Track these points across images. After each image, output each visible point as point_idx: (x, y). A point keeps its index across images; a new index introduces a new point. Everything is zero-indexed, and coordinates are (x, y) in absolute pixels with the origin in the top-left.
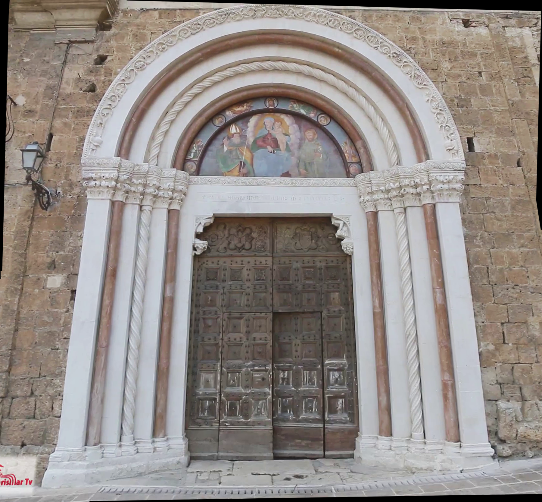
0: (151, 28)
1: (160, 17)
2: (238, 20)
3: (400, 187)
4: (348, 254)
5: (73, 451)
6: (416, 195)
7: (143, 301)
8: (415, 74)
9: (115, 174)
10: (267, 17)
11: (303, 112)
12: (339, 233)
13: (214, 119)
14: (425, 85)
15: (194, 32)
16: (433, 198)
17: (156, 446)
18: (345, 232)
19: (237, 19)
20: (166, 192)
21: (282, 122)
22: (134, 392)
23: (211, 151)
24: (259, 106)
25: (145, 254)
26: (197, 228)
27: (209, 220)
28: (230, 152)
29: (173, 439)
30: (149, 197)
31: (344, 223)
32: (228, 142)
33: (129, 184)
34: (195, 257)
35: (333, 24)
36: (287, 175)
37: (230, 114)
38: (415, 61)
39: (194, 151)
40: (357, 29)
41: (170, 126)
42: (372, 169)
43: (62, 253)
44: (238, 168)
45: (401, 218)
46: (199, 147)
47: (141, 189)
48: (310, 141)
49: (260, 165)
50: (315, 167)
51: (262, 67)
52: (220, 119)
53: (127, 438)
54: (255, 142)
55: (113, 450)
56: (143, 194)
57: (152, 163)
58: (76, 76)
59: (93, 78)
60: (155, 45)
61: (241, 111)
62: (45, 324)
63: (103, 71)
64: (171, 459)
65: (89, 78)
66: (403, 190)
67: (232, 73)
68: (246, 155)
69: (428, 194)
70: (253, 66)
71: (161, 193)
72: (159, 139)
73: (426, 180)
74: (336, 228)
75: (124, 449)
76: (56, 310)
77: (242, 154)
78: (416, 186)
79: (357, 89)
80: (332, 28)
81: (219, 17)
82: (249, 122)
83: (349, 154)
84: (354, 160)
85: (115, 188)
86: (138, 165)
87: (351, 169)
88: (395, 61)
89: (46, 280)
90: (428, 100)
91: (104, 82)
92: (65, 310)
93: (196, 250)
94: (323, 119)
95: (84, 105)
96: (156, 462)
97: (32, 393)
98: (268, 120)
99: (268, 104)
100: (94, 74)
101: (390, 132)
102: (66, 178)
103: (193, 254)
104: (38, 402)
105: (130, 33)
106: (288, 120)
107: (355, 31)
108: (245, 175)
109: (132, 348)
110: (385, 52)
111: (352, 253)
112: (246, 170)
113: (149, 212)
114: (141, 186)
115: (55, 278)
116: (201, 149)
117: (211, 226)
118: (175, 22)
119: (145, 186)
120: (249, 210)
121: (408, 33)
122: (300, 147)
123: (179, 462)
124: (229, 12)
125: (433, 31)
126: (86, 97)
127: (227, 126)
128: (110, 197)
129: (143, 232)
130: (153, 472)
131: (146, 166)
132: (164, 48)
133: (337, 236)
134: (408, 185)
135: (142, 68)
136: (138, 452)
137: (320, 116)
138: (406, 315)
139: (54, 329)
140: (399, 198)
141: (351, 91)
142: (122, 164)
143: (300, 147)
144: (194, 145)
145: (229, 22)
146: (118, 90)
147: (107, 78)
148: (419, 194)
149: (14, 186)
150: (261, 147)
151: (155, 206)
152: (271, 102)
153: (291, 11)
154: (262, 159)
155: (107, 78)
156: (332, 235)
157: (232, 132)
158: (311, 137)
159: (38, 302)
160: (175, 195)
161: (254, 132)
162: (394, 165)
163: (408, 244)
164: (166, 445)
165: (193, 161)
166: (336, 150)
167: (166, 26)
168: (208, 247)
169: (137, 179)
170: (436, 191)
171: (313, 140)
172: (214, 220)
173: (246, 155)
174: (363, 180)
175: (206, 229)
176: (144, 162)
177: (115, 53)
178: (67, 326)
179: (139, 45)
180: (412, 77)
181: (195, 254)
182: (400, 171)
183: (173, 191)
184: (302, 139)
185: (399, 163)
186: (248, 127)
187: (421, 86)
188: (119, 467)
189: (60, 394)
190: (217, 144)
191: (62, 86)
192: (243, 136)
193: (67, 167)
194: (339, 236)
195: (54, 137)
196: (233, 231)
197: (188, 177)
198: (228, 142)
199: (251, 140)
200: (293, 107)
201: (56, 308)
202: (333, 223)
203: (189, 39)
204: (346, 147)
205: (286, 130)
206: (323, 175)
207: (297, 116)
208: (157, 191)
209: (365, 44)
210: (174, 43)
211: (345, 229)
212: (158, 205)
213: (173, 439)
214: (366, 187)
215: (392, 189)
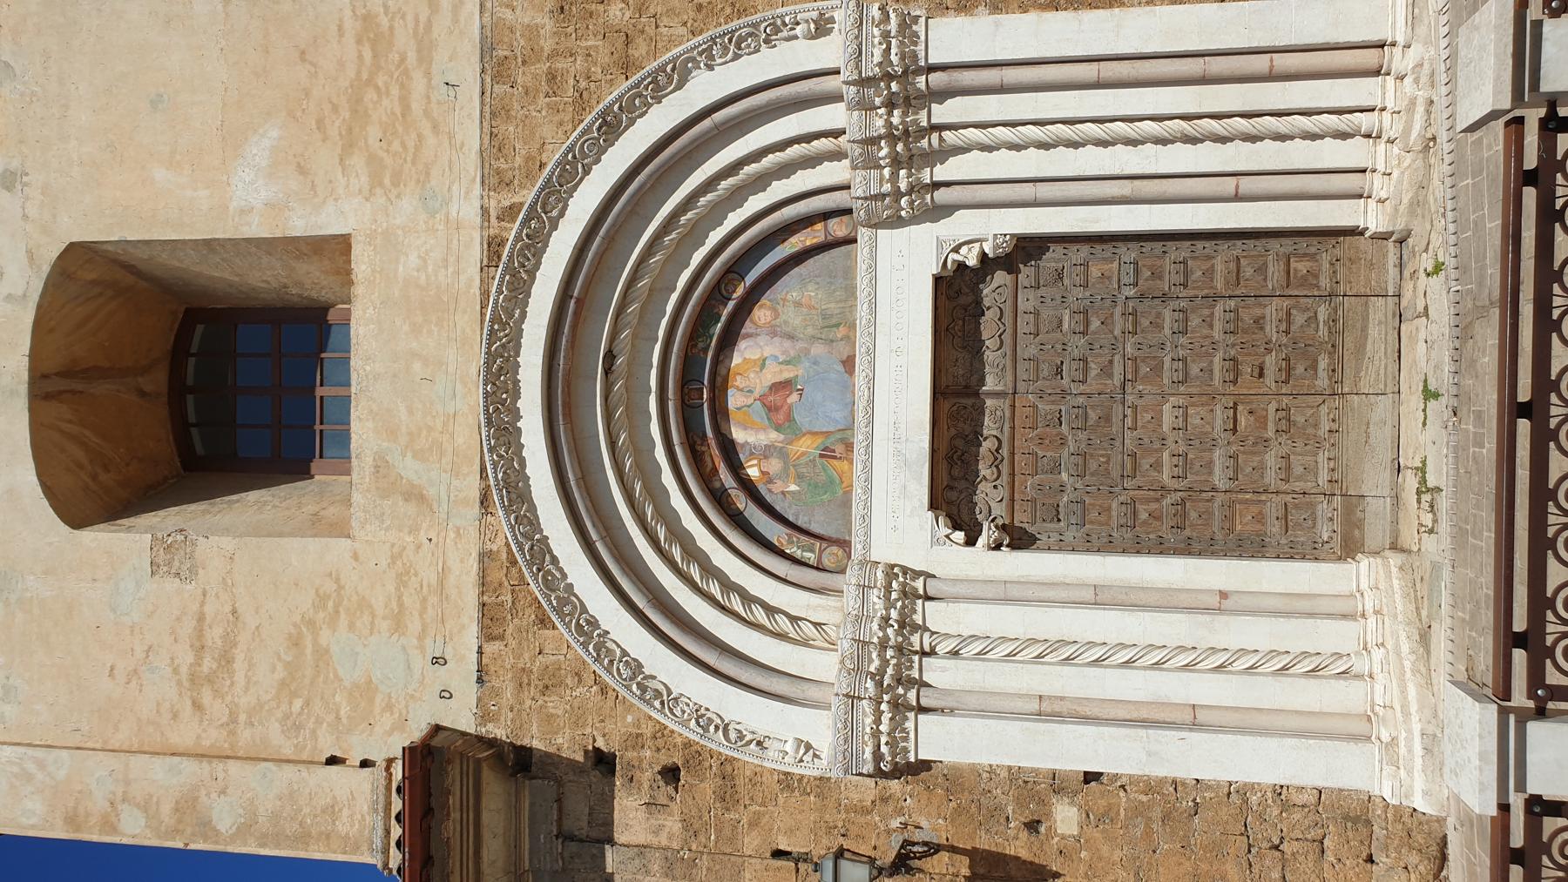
0: (526, 656)
1: (501, 637)
5: (1381, 762)
12: (972, 261)
28: (800, 478)
32: (779, 483)
34: (1013, 546)
36: (849, 364)
37: (726, 477)
43: (1010, 809)
44: (835, 462)
46: (790, 542)
48: (777, 316)
49: (827, 415)
50: (833, 307)
54: (778, 428)
58: (641, 814)
59: (648, 774)
62: (1148, 832)
63: (630, 754)
64: (1396, 582)
65: (646, 785)
68: (806, 446)
74: (961, 266)
76: (1122, 812)
77: (803, 454)
86: (842, 662)
89: (1063, 837)
91: (658, 750)
92: (1122, 794)
95: (707, 788)
96: (1400, 608)
97: (1276, 848)
98: (734, 400)
100: (638, 774)
102: (869, 812)
104: (1293, 835)
108: (849, 447)
111: (1012, 235)
112: (838, 447)
115: (1059, 818)
116: (796, 536)
123: (1401, 568)
125: (532, 31)
126: (691, 786)
130: (1419, 614)
139: (1157, 813)
146: (683, 712)
147: (649, 743)
150: (789, 418)
154: (816, 411)
155: (649, 743)
158: (768, 313)
159: (1105, 850)
161: (759, 429)
165: (821, 552)
171: (774, 310)
177: (588, 730)
178: (1151, 786)
188: (1409, 675)
189: (1278, 790)
191: (664, 842)
192: (766, 453)
193: (847, 812)
195: (781, 847)
198: (779, 483)
199: (774, 436)
201: (1118, 813)
205: (756, 361)
212: (918, 619)
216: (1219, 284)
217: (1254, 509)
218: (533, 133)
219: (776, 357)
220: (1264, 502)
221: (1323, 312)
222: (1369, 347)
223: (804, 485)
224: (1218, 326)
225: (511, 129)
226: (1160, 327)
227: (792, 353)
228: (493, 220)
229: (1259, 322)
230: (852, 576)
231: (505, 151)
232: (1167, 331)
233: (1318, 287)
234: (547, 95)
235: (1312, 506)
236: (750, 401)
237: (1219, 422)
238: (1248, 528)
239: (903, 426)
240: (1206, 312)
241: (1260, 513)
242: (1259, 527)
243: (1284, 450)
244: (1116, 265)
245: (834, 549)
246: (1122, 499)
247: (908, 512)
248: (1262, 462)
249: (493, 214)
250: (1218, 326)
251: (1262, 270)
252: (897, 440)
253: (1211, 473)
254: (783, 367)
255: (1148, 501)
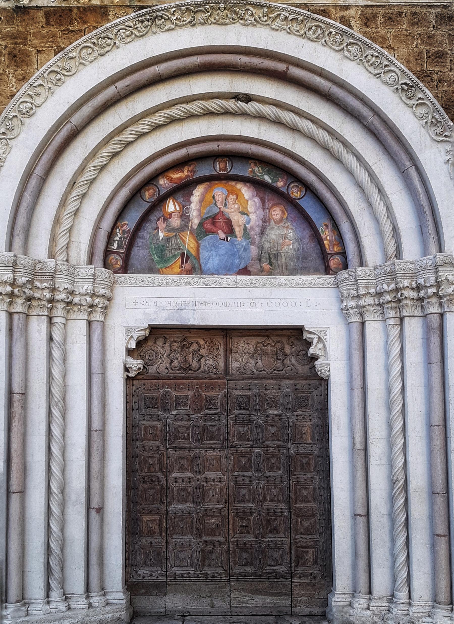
0: (36, 42)
1: (48, 23)
2: (169, 30)
3: (397, 290)
4: (323, 378)
6: (417, 300)
7: (64, 436)
8: (433, 117)
9: (9, 276)
10: (212, 23)
11: (267, 179)
12: (312, 351)
13: (143, 191)
14: (446, 136)
15: (103, 51)
16: (441, 304)
17: (91, 601)
18: (320, 349)
19: (167, 27)
20: (83, 298)
21: (238, 194)
22: (60, 542)
23: (142, 238)
24: (204, 170)
25: (61, 381)
26: (127, 343)
27: (142, 333)
28: (168, 240)
29: (111, 592)
30: (61, 306)
31: (319, 338)
33: (30, 289)
34: (128, 378)
35: (314, 34)
36: (245, 271)
38: (436, 97)
39: (117, 238)
40: (351, 44)
41: (81, 202)
42: (362, 263)
44: (179, 263)
45: (395, 332)
46: (124, 232)
47: (47, 295)
51: (208, 109)
52: (151, 191)
53: (55, 595)
54: (201, 224)
55: (40, 607)
56: (51, 301)
57: (60, 258)
60: (46, 75)
61: (180, 178)
66: (399, 294)
67: (165, 120)
68: (189, 243)
69: (434, 300)
70: (194, 107)
71: (76, 300)
72: (66, 223)
73: (432, 280)
74: (309, 344)
75: (53, 605)
77: (184, 242)
78: (418, 288)
79: (345, 144)
80: (312, 41)
81: (139, 25)
82: (192, 194)
83: (328, 255)
84: (336, 249)
85: (11, 295)
86: (40, 262)
87: (331, 263)
88: (404, 98)
90: (448, 160)
93: (128, 372)
94: (295, 190)
98: (219, 192)
99: (219, 167)
101: (389, 209)
103: (126, 377)
105: (4, 52)
106: (246, 191)
107: (347, 46)
108: (190, 272)
109: (54, 493)
110: (391, 82)
111: (329, 376)
112: (192, 266)
113: (62, 326)
114: (48, 291)
117: (146, 339)
118: (72, 31)
119: (53, 290)
120: (194, 319)
121: (430, 45)
122: (262, 232)
124: (154, 15)
127: (161, 200)
128: (5, 308)
129: (56, 353)
131: (51, 263)
132: (59, 80)
133: (309, 355)
134: (408, 287)
135: (29, 113)
136: (70, 608)
137: (292, 185)
138: (395, 494)
140: (394, 305)
141: (336, 146)
142: (18, 262)
143: (262, 232)
144: (118, 231)
145: (154, 33)
148: (421, 300)
149: (259, 133)
150: (208, 232)
151: (69, 317)
152: (222, 165)
153: (249, 12)
156: (304, 352)
157: (170, 210)
158: (278, 217)
160: (97, 301)
162: (390, 258)
163: (403, 367)
164: (103, 600)
165: (118, 253)
166: (312, 235)
167: (59, 40)
168: (144, 367)
169: (41, 282)
170: (445, 296)
171: (281, 220)
172: (151, 332)
173: (189, 243)
174: (347, 279)
175: (139, 343)
176: (49, 258)
179: (20, 72)
180: (429, 124)
181: (128, 376)
182: (397, 268)
183: (93, 295)
184: (266, 220)
185: (398, 254)
186: (191, 203)
187: (441, 138)
190: (148, 227)
192: (184, 216)
194: (312, 354)
196: (176, 346)
197: (112, 276)
200: (253, 171)
202: (304, 338)
203: (95, 64)
204: (327, 232)
205: (244, 206)
206: (293, 272)
207: (258, 185)
208: (70, 297)
209: (360, 69)
210: (73, 71)
211: (320, 345)
213: (111, 592)
214: (349, 289)
215: (385, 291)
216: (298, 505)
217: (156, 529)
218: (401, 42)
219: (249, 222)
220: (161, 535)
221: (281, 569)
222: (260, 597)
223: (163, 243)
224: (271, 505)
225: (405, 26)
226: (271, 469)
227: (252, 233)
228: (341, 14)
229: (275, 530)
230: (103, 273)
231: (389, 22)
232: (268, 474)
233: (297, 566)
234: (428, 51)
235: (159, 564)
236: (219, 205)
237: (211, 506)
238: (145, 525)
239: (204, 307)
240: (281, 498)
241: (154, 533)
242: (146, 532)
243: (194, 547)
244: (310, 441)
245: (120, 263)
246: (161, 447)
247: (147, 311)
248: (186, 533)
249: (346, 13)
250: (271, 505)
251: (308, 531)
252: (195, 304)
253: (179, 502)
254: (242, 228)
255: (160, 463)
